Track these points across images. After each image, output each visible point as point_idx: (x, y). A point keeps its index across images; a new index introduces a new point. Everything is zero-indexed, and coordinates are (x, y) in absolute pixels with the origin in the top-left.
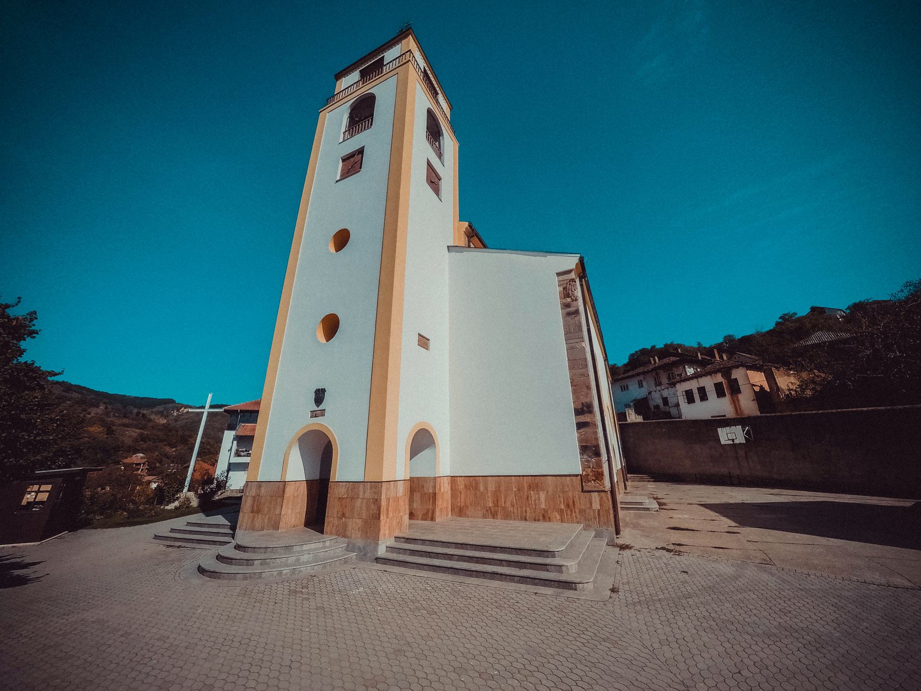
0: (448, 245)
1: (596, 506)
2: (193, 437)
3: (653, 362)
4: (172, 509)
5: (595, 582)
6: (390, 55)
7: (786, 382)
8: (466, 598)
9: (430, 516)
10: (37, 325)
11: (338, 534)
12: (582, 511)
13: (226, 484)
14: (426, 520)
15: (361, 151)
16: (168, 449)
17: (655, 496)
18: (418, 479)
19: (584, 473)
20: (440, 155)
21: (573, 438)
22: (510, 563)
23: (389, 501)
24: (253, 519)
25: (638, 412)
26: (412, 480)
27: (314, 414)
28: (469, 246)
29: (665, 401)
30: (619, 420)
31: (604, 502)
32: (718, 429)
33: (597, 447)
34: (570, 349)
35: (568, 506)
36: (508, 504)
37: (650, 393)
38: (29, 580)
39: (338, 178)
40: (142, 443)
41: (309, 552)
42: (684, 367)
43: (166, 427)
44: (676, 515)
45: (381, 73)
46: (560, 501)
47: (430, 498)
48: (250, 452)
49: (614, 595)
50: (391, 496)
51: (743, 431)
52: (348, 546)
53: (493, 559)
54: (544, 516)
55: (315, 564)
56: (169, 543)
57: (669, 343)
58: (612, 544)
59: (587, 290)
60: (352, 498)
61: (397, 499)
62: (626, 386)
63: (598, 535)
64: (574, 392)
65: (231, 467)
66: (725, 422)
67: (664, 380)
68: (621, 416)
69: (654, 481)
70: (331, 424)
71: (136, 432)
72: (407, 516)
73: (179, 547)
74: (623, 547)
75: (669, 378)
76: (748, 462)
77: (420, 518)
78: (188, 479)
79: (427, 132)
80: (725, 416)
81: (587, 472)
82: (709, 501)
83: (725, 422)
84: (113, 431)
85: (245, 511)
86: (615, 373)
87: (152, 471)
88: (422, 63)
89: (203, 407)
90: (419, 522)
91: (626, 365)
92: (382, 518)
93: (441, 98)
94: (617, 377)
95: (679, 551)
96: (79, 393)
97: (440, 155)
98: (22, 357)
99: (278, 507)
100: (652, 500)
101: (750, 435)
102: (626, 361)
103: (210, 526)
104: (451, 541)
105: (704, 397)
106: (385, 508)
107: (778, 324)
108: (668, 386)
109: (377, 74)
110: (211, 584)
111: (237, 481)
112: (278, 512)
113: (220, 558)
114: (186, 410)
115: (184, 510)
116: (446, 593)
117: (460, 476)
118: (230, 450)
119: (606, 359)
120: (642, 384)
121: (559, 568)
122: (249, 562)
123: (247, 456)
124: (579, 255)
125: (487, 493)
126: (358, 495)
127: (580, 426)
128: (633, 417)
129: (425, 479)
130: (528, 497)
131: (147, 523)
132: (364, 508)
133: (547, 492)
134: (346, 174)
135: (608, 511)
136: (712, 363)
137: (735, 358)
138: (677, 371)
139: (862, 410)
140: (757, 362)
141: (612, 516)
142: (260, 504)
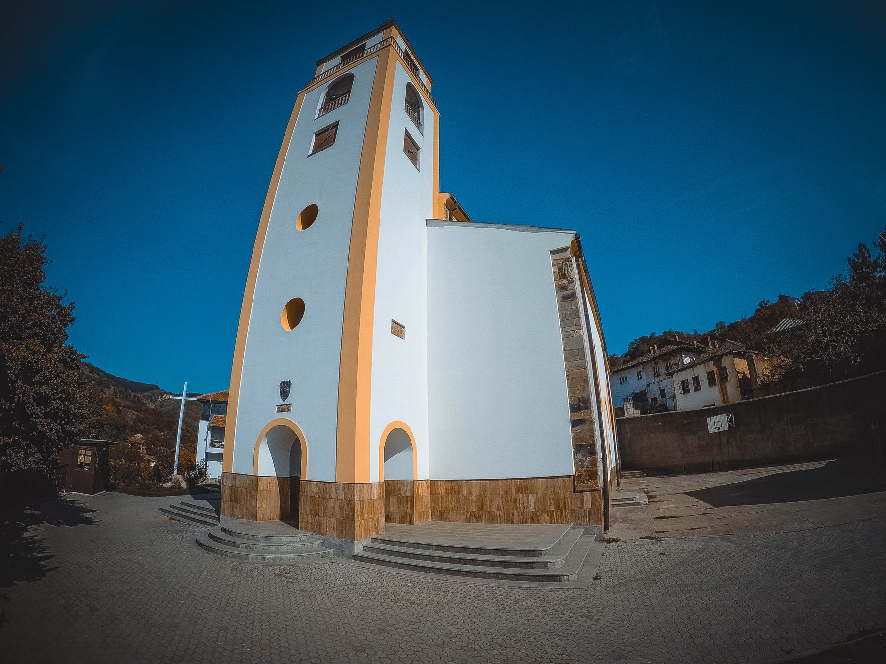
0: (427, 219)
1: (588, 505)
2: (175, 424)
3: (652, 352)
4: (168, 488)
5: (579, 574)
6: (370, 43)
7: (763, 368)
8: (448, 593)
9: (408, 519)
10: (75, 314)
11: (313, 530)
12: (572, 512)
13: (206, 472)
14: (404, 523)
15: (335, 126)
16: (157, 432)
17: (646, 490)
18: (394, 482)
19: (578, 473)
20: (419, 125)
21: (567, 435)
22: (493, 563)
23: (363, 504)
24: (233, 509)
25: (636, 406)
26: (387, 483)
27: (281, 409)
28: (451, 220)
29: (663, 392)
30: (617, 415)
31: (597, 500)
32: (708, 419)
33: (593, 445)
34: (567, 338)
35: (558, 507)
36: (494, 508)
37: (648, 385)
38: (93, 522)
39: (310, 153)
40: (140, 424)
41: (287, 543)
42: (682, 356)
43: (155, 413)
44: (663, 506)
45: (362, 56)
46: (551, 503)
47: (408, 502)
48: (223, 443)
49: (596, 582)
50: (366, 498)
51: (728, 418)
52: (324, 543)
53: (477, 560)
54: (532, 519)
55: (295, 555)
56: (172, 516)
57: (668, 331)
58: (600, 539)
59: (584, 271)
60: (324, 498)
61: (371, 502)
62: (625, 378)
63: (587, 532)
64: (571, 386)
65: (209, 456)
66: (713, 411)
67: (663, 371)
68: (618, 411)
69: (646, 476)
70: (297, 419)
71: (134, 414)
72: (383, 519)
73: (179, 521)
74: (609, 541)
75: (667, 369)
76: (728, 447)
77: (398, 520)
78: (176, 463)
79: (405, 104)
80: (714, 405)
81: (581, 472)
82: (693, 489)
83: (713, 411)
84: (120, 411)
85: (225, 499)
86: (612, 363)
87: (150, 451)
88: (403, 46)
89: (181, 395)
90: (397, 525)
91: (626, 355)
92: (356, 519)
93: (422, 74)
94: (616, 369)
95: (661, 537)
96: (98, 375)
97: (419, 125)
98: (695, 331)
99: (254, 500)
100: (643, 494)
101: (732, 423)
102: (626, 351)
103: (198, 508)
104: (431, 543)
105: (697, 388)
106: (360, 512)
107: (757, 311)
108: (666, 377)
109: (358, 57)
110: (208, 556)
111: (215, 471)
112: (254, 504)
113: (211, 536)
114: (168, 397)
115: (176, 491)
116: (428, 588)
117: (441, 480)
118: (206, 440)
119: (605, 349)
120: (641, 375)
121: (545, 565)
122: (236, 545)
123: (221, 447)
124: (574, 232)
125: (471, 497)
126: (330, 495)
127: (575, 423)
128: (631, 412)
129: (402, 482)
130: (516, 500)
131: (150, 495)
132: (337, 509)
133: (537, 495)
134: (318, 148)
135: (598, 510)
136: (706, 351)
137: (725, 346)
138: (674, 361)
139: (807, 390)
140: (741, 350)
141: (603, 513)
142: (237, 495)
